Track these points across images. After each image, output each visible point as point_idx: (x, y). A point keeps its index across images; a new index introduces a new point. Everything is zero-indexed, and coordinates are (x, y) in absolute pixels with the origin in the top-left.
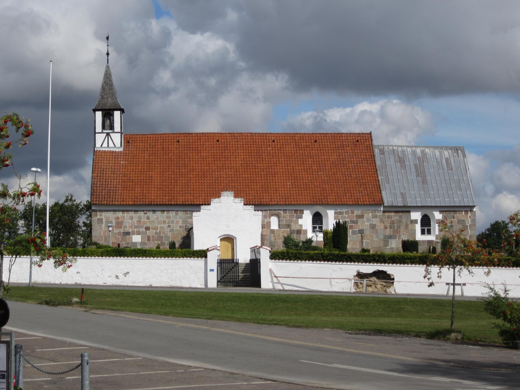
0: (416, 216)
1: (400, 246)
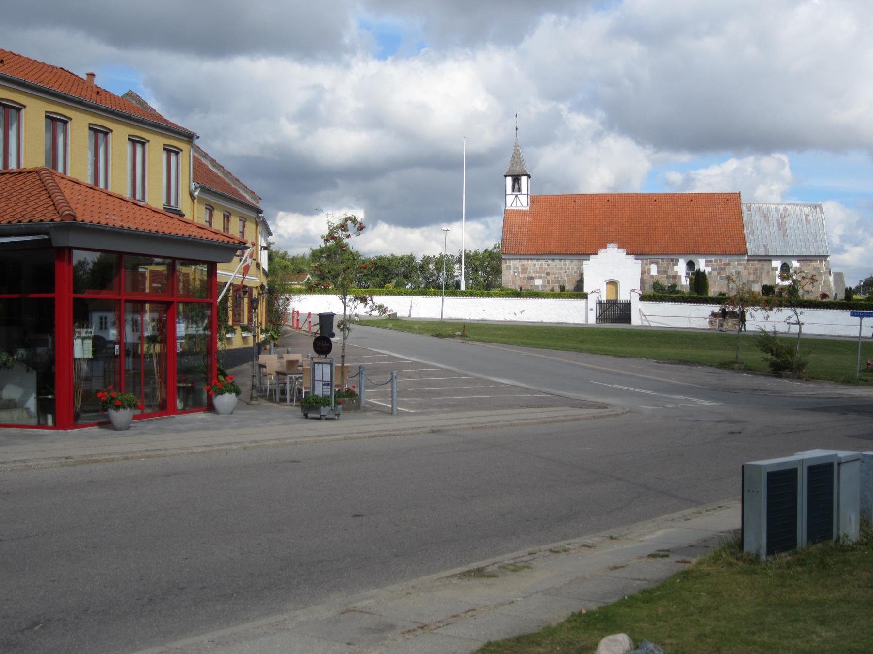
0: (777, 264)
1: (761, 289)
